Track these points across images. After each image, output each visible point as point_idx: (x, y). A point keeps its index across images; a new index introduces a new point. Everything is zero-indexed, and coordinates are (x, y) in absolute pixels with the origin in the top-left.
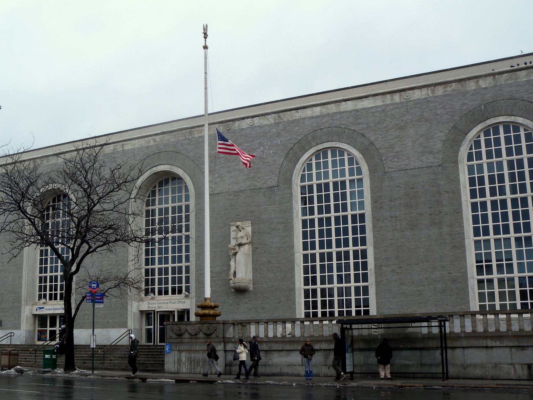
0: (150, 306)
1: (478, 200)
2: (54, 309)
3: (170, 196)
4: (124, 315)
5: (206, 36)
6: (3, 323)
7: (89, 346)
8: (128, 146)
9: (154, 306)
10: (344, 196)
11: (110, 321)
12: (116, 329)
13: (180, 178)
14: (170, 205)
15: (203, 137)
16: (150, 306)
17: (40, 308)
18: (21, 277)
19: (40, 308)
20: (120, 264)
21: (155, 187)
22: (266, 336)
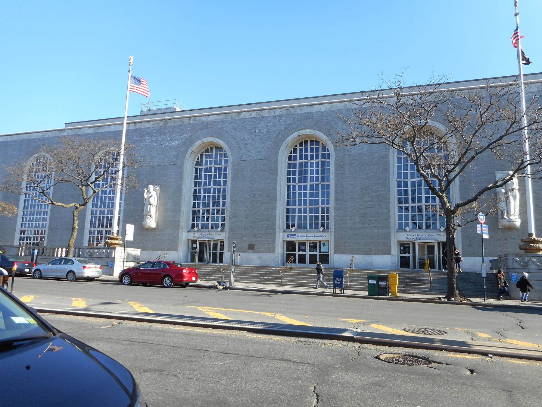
0: (408, 237)
1: (403, 180)
2: (306, 236)
3: (213, 159)
4: (388, 243)
5: (516, 6)
6: (255, 246)
7: (480, 274)
8: (315, 109)
9: (413, 237)
10: (306, 172)
11: (373, 248)
12: (379, 256)
13: (221, 148)
14: (213, 166)
15: (121, 132)
16: (408, 237)
17: (292, 235)
18: (275, 208)
19: (292, 235)
20: (381, 201)
21: (203, 152)
22: (62, 249)
